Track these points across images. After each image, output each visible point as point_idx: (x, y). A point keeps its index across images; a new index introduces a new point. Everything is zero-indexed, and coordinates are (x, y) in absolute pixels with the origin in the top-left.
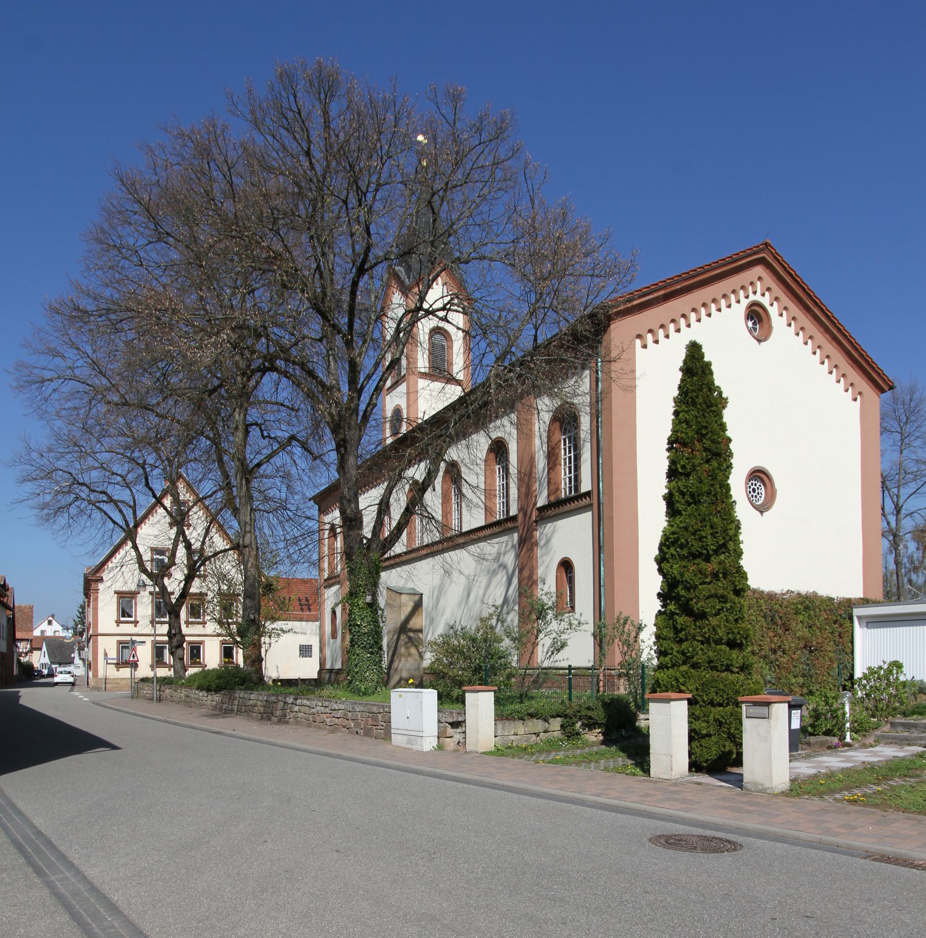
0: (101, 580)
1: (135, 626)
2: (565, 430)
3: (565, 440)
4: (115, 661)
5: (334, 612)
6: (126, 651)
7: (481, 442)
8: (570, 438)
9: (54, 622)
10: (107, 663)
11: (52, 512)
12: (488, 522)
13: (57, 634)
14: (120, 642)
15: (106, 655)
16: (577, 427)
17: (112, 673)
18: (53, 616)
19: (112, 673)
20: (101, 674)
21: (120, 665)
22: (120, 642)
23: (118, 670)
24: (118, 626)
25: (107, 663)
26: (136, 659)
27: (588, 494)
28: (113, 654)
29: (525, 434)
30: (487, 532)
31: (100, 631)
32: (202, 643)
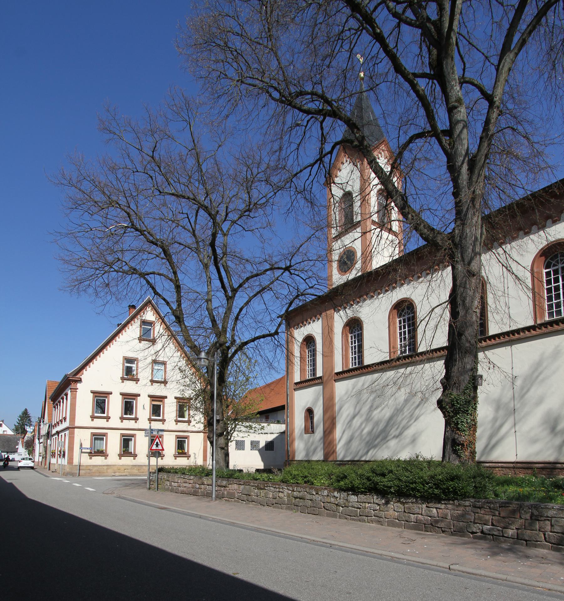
0: (80, 381)
1: (107, 421)
2: (352, 330)
3: (352, 337)
4: (89, 451)
5: (310, 412)
6: (98, 442)
7: (339, 319)
8: (355, 336)
9: (3, 425)
10: (82, 452)
11: (78, 285)
12: (303, 380)
13: (5, 433)
14: (93, 434)
15: (81, 445)
16: (315, 345)
17: (86, 460)
18: (3, 421)
19: (86, 460)
20: (76, 461)
21: (91, 454)
22: (93, 434)
23: (91, 458)
24: (92, 420)
25: (82, 452)
26: (160, 447)
27: (320, 378)
28: (87, 444)
29: (328, 332)
30: (346, 375)
31: (77, 424)
32: (187, 437)
